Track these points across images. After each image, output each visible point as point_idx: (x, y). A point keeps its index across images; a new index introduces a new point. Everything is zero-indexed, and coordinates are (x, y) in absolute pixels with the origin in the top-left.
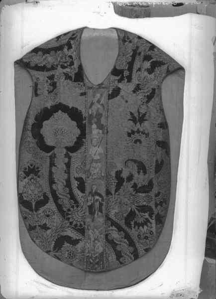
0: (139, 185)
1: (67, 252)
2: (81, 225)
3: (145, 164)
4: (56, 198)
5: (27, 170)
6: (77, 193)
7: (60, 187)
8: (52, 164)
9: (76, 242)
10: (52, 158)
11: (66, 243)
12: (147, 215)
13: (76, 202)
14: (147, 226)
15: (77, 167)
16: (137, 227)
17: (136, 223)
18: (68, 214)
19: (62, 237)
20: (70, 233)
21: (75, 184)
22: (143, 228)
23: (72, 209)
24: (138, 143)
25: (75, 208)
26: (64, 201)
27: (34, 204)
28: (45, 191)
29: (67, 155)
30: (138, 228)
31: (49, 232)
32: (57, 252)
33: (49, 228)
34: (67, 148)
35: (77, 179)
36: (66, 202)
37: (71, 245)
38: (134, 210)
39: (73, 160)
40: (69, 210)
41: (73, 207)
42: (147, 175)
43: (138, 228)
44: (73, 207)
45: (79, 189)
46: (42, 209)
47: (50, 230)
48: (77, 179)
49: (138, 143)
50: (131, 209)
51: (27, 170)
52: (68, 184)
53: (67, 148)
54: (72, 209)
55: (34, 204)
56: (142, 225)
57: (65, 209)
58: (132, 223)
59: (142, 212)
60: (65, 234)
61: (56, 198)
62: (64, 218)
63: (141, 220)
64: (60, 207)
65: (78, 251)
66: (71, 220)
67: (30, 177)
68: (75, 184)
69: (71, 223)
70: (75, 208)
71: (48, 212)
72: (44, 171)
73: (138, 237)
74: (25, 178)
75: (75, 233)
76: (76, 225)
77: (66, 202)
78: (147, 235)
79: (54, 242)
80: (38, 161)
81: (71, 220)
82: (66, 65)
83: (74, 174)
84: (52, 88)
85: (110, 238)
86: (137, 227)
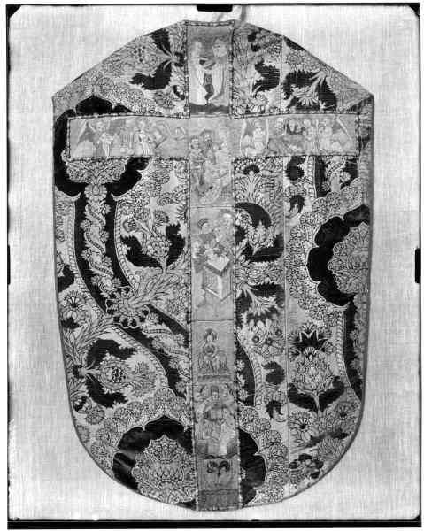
0: (256, 249)
1: (111, 371)
2: (134, 323)
3: (266, 210)
4: (87, 274)
5: (309, 336)
6: (128, 267)
7: (97, 259)
8: (80, 217)
9: (127, 353)
10: (82, 204)
11: (108, 354)
12: (271, 300)
13: (125, 282)
14: (272, 320)
15: (126, 221)
16: (252, 322)
17: (250, 317)
18: (110, 304)
19: (100, 341)
20: (113, 335)
21: (122, 250)
22: (264, 323)
23: (117, 295)
24: (251, 173)
25: (123, 292)
26: (103, 280)
27: (317, 400)
28: (336, 374)
29: (109, 201)
30: (255, 325)
31: (77, 332)
32: (92, 368)
33: (77, 326)
34: (108, 185)
35: (125, 241)
36: (107, 284)
37: (118, 359)
38: (248, 295)
39: (118, 209)
40: (112, 296)
41: (119, 291)
42: (271, 229)
43: (255, 325)
44: (119, 291)
45: (129, 259)
46: (332, 406)
47: (80, 329)
48: (125, 241)
49: (251, 173)
50: (243, 292)
51: (309, 336)
52: (110, 252)
53: (108, 185)
54: (117, 295)
55: (317, 400)
56: (262, 318)
57: (106, 295)
58: (244, 316)
59: (262, 296)
60: (104, 337)
61: (87, 274)
62: (105, 310)
63: (261, 310)
64: (95, 292)
65: (130, 369)
66: (116, 314)
67: (307, 351)
68: (122, 250)
69: (117, 319)
70: (123, 292)
71: (78, 300)
72: (336, 338)
73: (253, 340)
74: (297, 354)
75: (121, 334)
76: (125, 323)
77: (107, 284)
78: (270, 336)
79: (87, 351)
80: (319, 323)
81: (116, 314)
82: (314, 464)
83: (121, 232)
84: (347, 177)
85: (182, 337)
86: (252, 322)
